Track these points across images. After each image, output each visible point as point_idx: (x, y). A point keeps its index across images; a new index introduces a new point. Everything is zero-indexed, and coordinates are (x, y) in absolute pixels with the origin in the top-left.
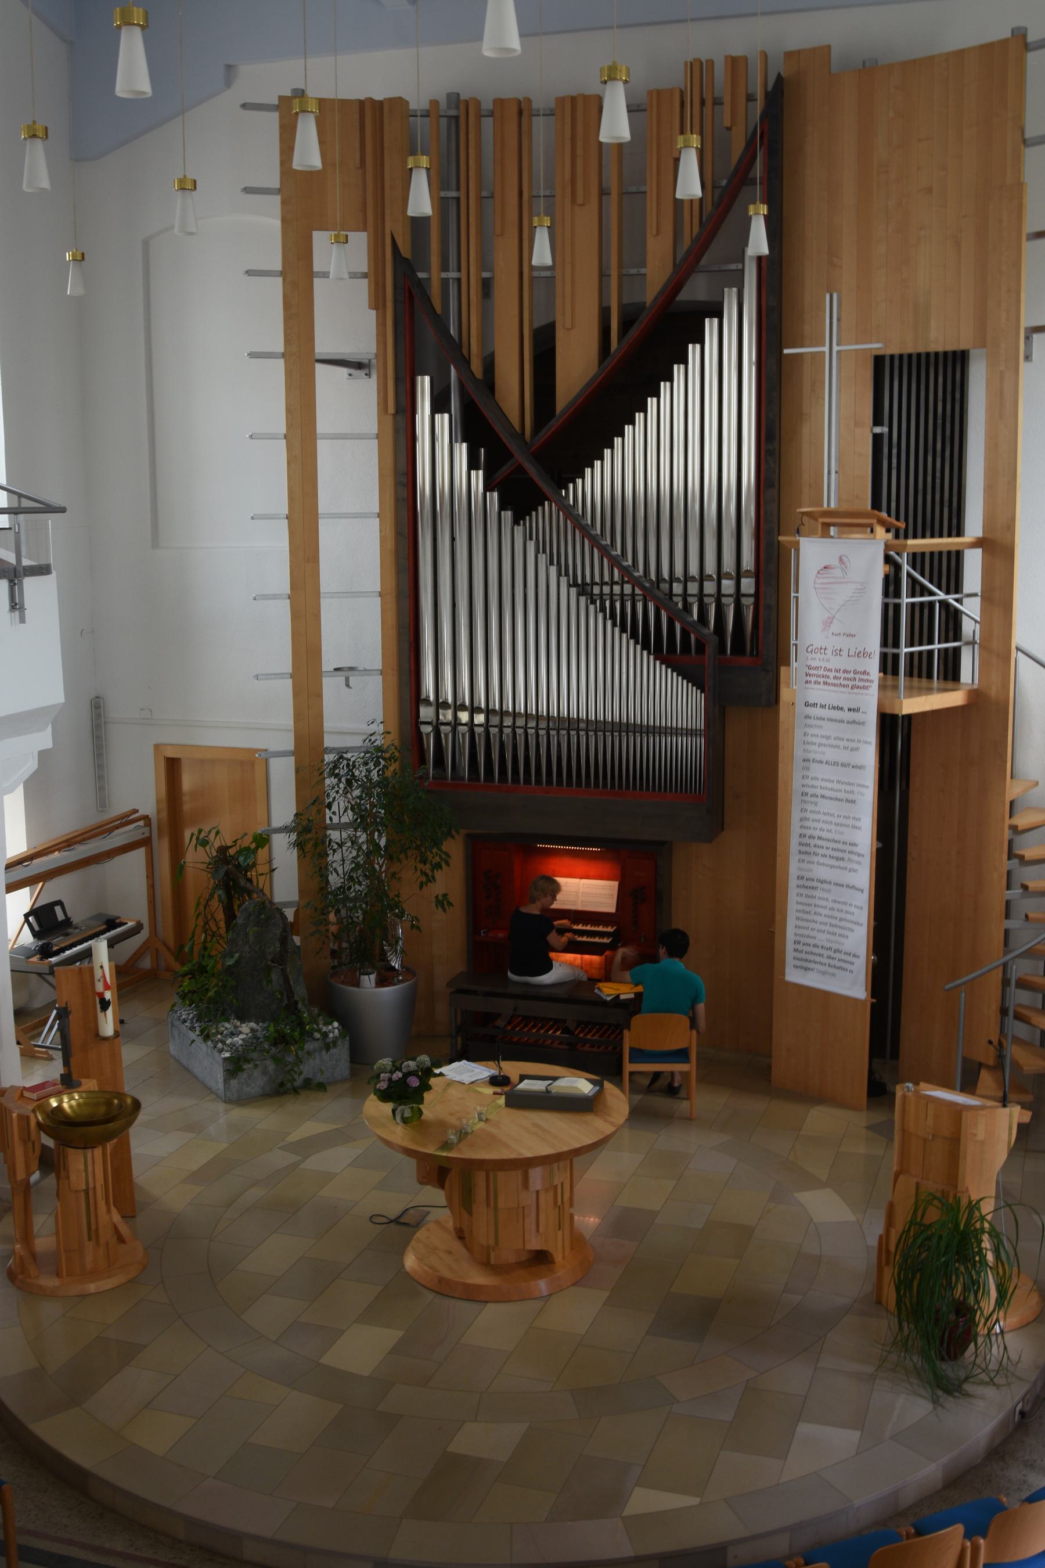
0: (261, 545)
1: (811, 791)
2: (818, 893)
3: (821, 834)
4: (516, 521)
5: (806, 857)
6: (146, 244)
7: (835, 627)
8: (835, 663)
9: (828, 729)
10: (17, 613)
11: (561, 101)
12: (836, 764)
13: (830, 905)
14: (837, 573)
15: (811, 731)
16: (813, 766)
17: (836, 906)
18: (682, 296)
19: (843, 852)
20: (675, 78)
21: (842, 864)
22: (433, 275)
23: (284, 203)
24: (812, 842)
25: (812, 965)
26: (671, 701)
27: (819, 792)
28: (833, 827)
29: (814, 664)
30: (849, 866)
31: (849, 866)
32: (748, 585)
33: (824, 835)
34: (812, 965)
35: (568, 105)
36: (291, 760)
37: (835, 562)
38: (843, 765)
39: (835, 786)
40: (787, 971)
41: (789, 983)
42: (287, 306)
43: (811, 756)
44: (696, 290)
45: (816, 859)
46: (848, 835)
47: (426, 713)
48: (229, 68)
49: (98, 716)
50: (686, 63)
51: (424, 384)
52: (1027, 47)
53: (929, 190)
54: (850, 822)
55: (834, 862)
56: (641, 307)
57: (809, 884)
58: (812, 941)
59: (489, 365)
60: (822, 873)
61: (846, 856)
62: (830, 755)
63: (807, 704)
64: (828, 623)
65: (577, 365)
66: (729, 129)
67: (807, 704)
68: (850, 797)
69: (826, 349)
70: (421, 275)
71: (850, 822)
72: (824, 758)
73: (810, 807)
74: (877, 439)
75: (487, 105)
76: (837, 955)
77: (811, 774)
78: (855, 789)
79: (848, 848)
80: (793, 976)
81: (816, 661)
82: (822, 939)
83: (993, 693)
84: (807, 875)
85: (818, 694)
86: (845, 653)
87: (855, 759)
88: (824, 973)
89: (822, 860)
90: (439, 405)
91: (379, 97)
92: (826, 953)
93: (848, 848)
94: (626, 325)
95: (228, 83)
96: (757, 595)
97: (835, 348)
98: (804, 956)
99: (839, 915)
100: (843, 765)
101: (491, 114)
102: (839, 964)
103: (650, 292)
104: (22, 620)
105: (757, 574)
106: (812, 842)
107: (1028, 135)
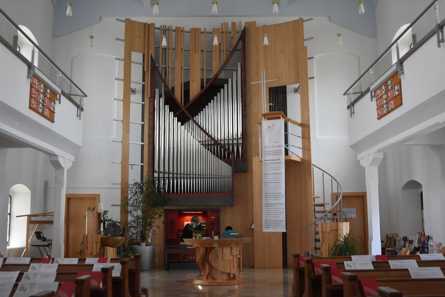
0: (100, 138)
1: (267, 182)
2: (270, 207)
3: (270, 192)
4: (182, 125)
5: (267, 199)
6: (72, 59)
7: (272, 141)
8: (272, 149)
9: (271, 166)
10: (78, 117)
11: (192, 29)
12: (274, 174)
13: (274, 210)
14: (272, 128)
15: (266, 167)
16: (267, 175)
17: (276, 210)
18: (218, 77)
19: (276, 196)
20: (219, 26)
21: (277, 198)
22: (161, 66)
23: (125, 43)
24: (268, 194)
25: (269, 226)
26: (225, 169)
27: (269, 182)
28: (274, 190)
29: (266, 150)
30: (279, 198)
31: (279, 198)
32: (240, 141)
33: (272, 192)
34: (269, 226)
35: (194, 32)
36: (197, 118)
37: (271, 125)
38: (276, 174)
39: (274, 179)
40: (263, 229)
41: (264, 232)
42: (125, 68)
43: (267, 173)
44: (222, 76)
45: (269, 199)
46: (278, 191)
47: (156, 175)
48: (100, 18)
49: (47, 186)
50: (222, 24)
51: (157, 91)
52: (303, 21)
53: (282, 51)
54: (278, 188)
55: (275, 199)
56: (210, 79)
57: (268, 205)
58: (269, 220)
59: (173, 88)
60: (272, 202)
61: (278, 196)
62: (272, 172)
63: (265, 161)
64: (270, 140)
65: (195, 90)
66: (232, 38)
67: (265, 161)
68: (278, 181)
69: (262, 82)
70: (157, 65)
71: (278, 188)
72: (270, 173)
73: (267, 186)
74: (270, 106)
75: (174, 28)
76: (277, 222)
77: (267, 178)
78: (279, 179)
79: (278, 194)
80: (265, 230)
81: (267, 150)
82: (272, 219)
83: (306, 159)
84: (267, 203)
85: (268, 157)
86: (275, 147)
87: (279, 172)
88: (273, 228)
89: (271, 199)
90: (160, 96)
91: (149, 23)
92: (274, 222)
93: (278, 194)
94: (207, 83)
95: (100, 21)
96: (243, 144)
97: (265, 81)
98: (268, 224)
99: (277, 212)
100: (276, 174)
101: (175, 31)
102: (277, 224)
103: (212, 76)
104: (80, 119)
105: (243, 139)
106: (268, 194)
107: (305, 38)
